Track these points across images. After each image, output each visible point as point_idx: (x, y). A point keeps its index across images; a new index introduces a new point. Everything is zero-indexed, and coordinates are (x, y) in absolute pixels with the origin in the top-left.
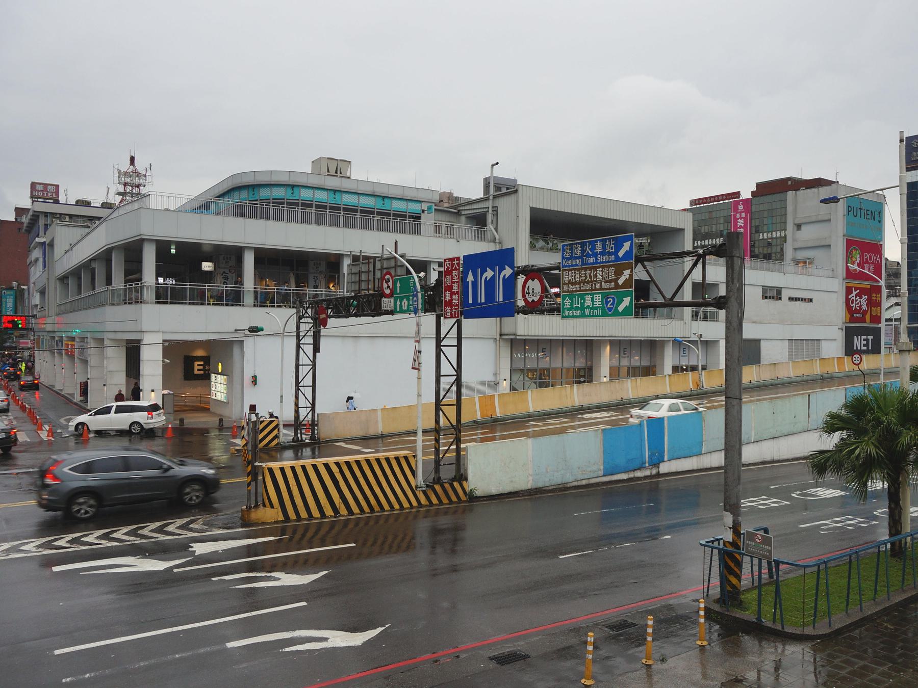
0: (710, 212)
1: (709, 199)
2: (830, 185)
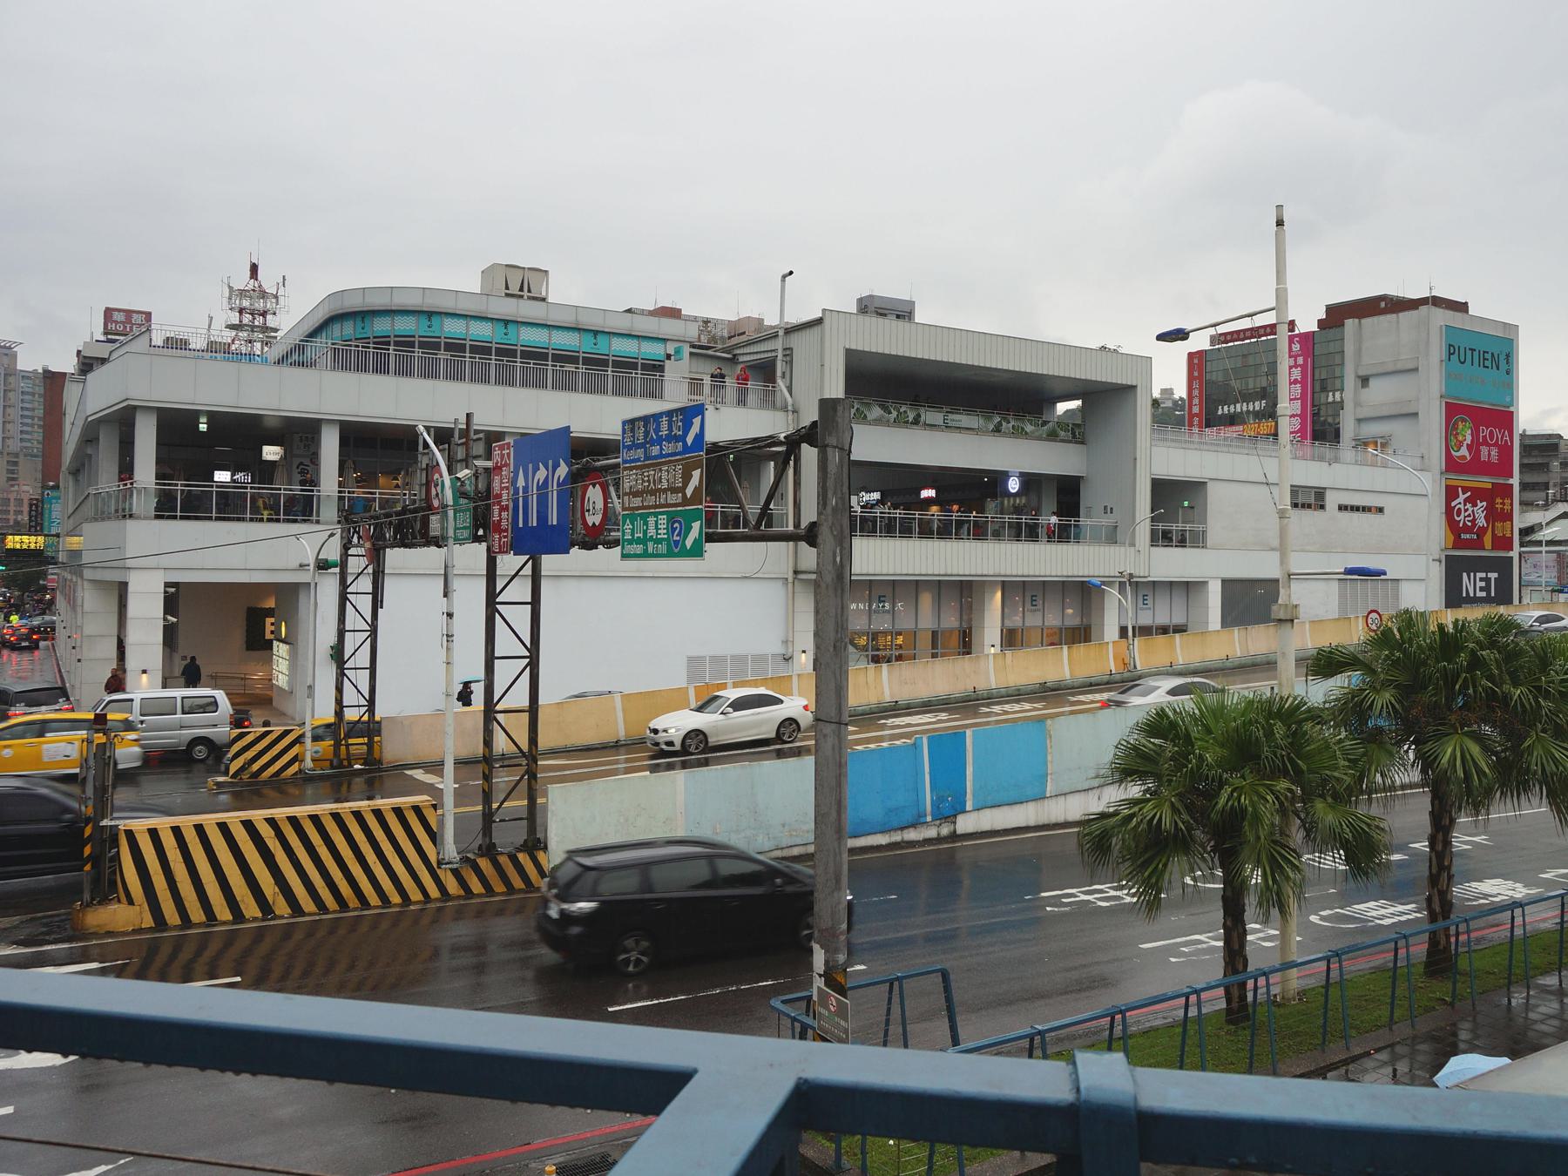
1: (1242, 333)
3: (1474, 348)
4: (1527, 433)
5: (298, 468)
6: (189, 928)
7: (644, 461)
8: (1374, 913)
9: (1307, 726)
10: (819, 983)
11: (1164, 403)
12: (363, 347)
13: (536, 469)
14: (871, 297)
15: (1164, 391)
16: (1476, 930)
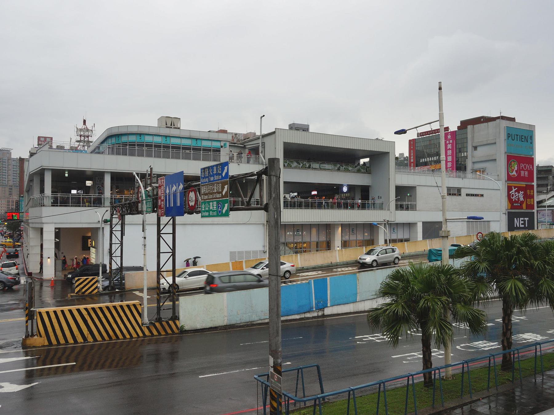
0: (430, 140)
2: (495, 120)
3: (518, 134)
4: (539, 166)
5: (97, 188)
6: (60, 345)
7: (208, 183)
8: (481, 346)
9: (454, 276)
10: (272, 370)
11: (401, 158)
12: (118, 146)
13: (172, 186)
14: (294, 124)
15: (400, 154)
16: (521, 353)
